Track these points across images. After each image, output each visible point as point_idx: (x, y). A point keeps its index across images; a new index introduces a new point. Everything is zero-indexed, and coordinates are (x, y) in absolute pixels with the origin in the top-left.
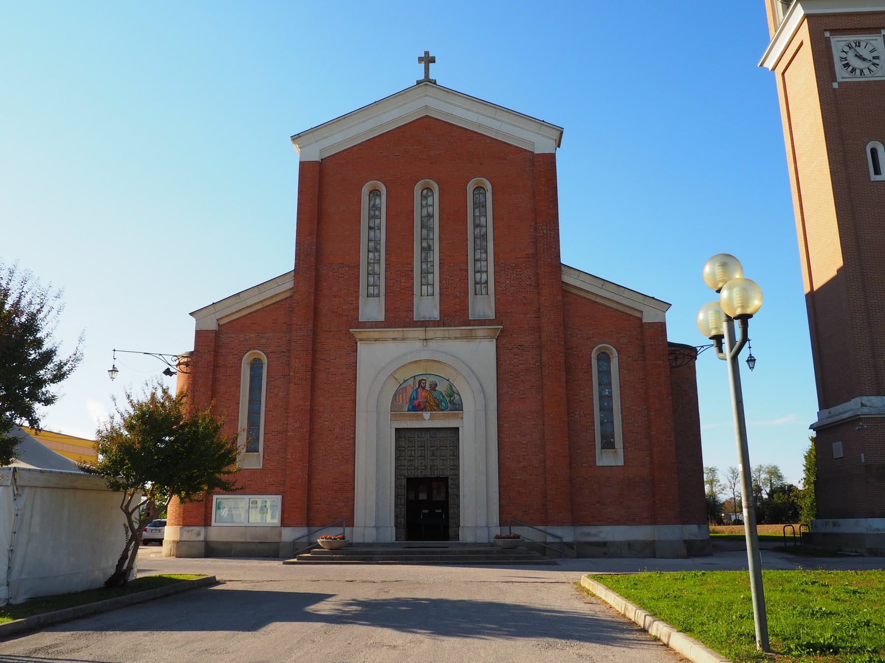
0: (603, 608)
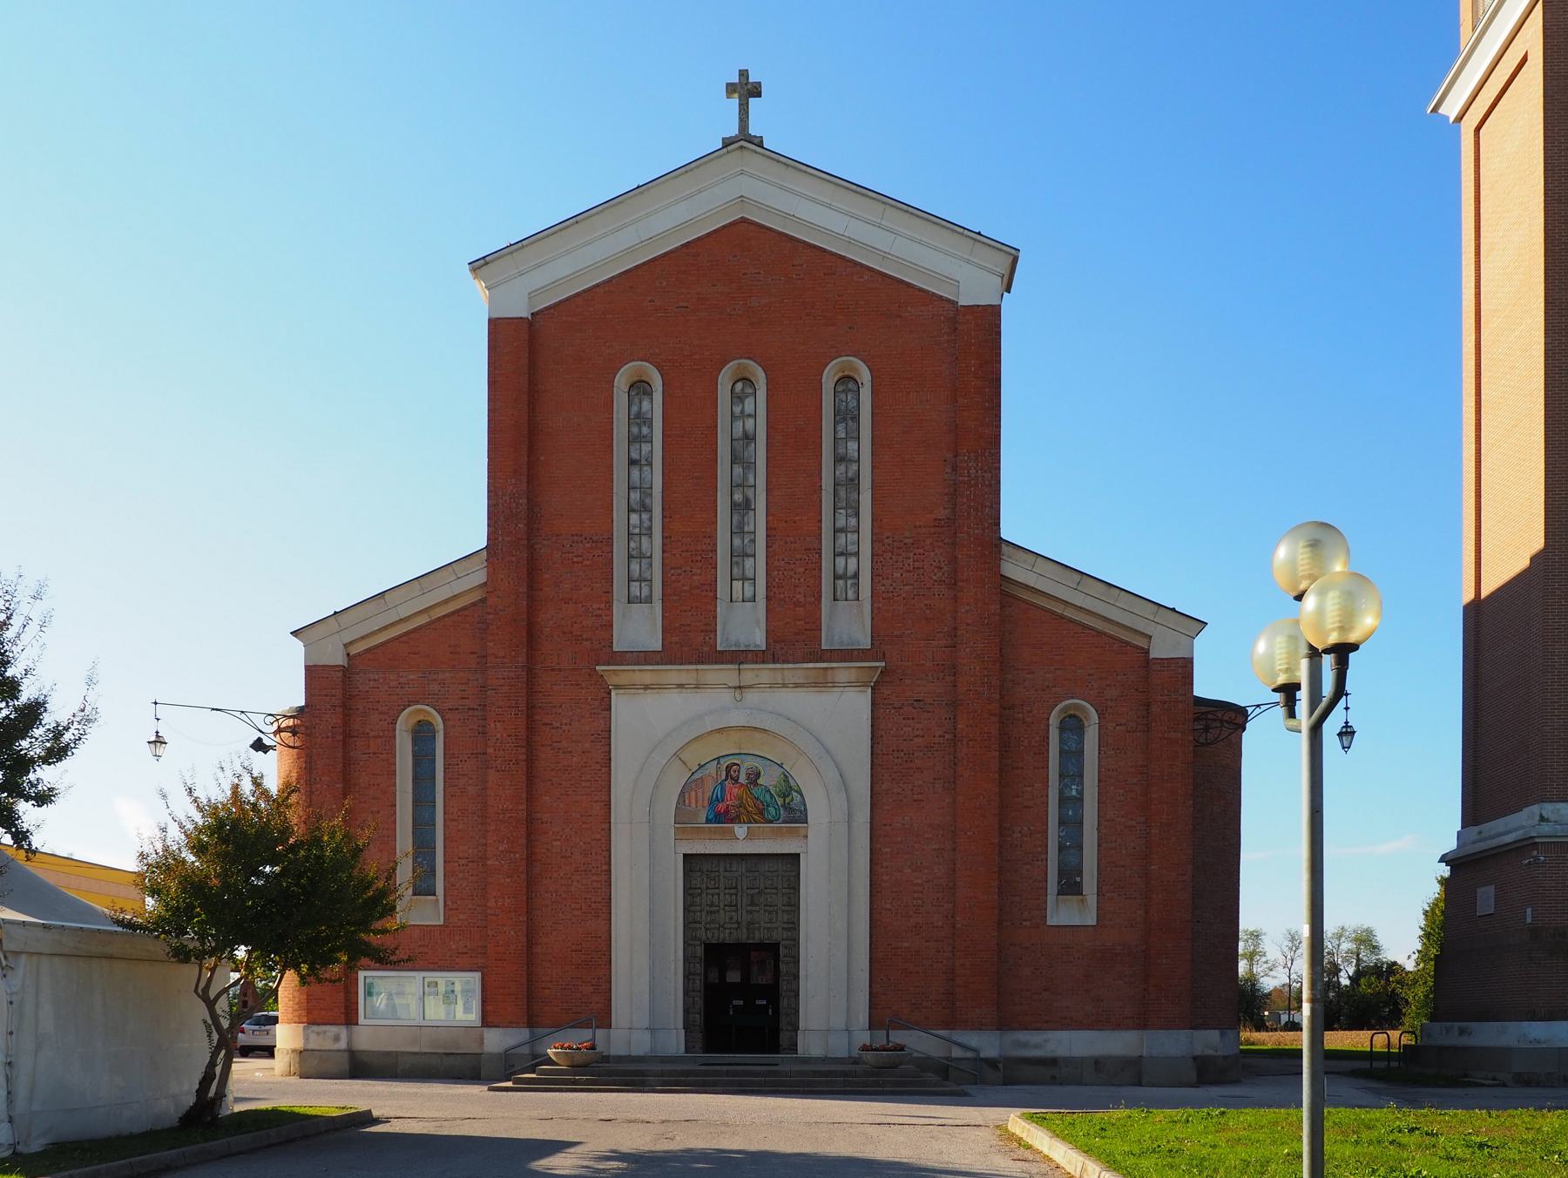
0: (1044, 1167)
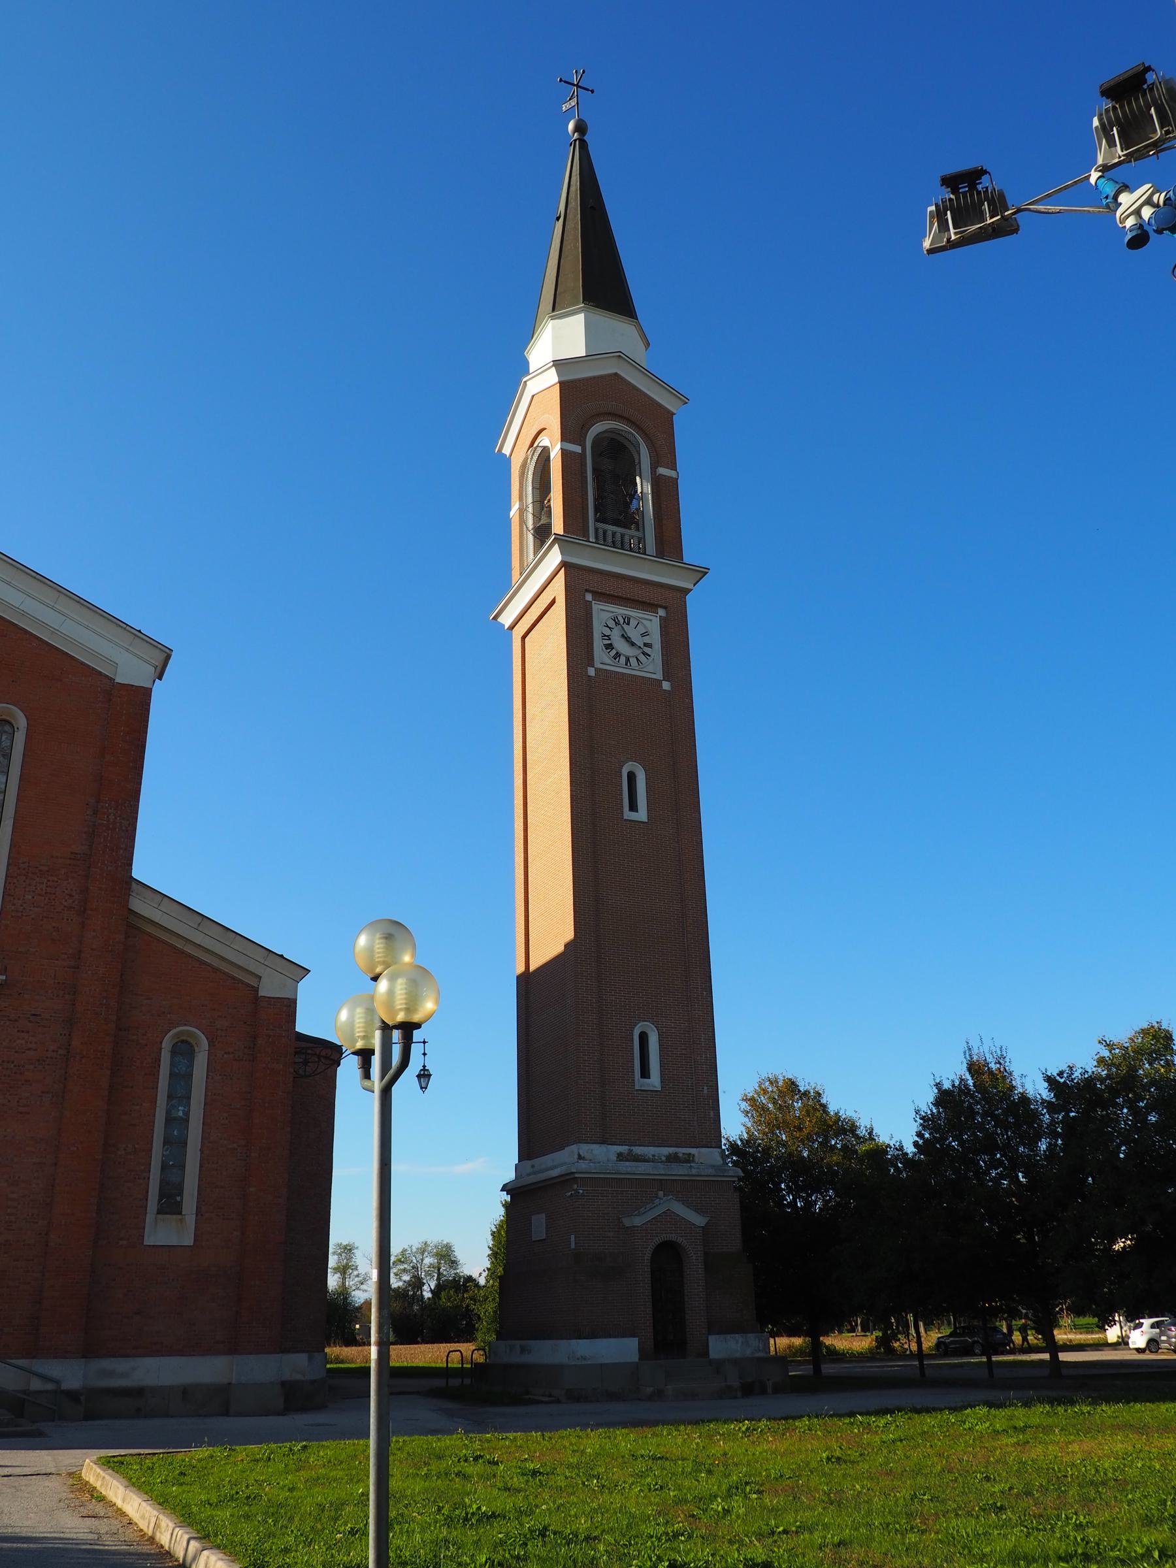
0: (115, 1524)
